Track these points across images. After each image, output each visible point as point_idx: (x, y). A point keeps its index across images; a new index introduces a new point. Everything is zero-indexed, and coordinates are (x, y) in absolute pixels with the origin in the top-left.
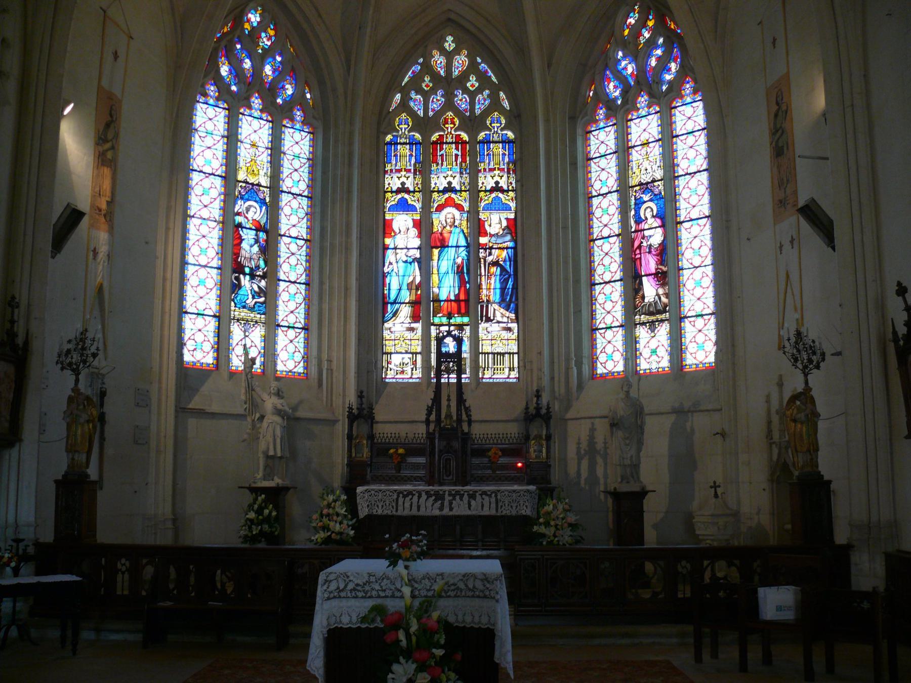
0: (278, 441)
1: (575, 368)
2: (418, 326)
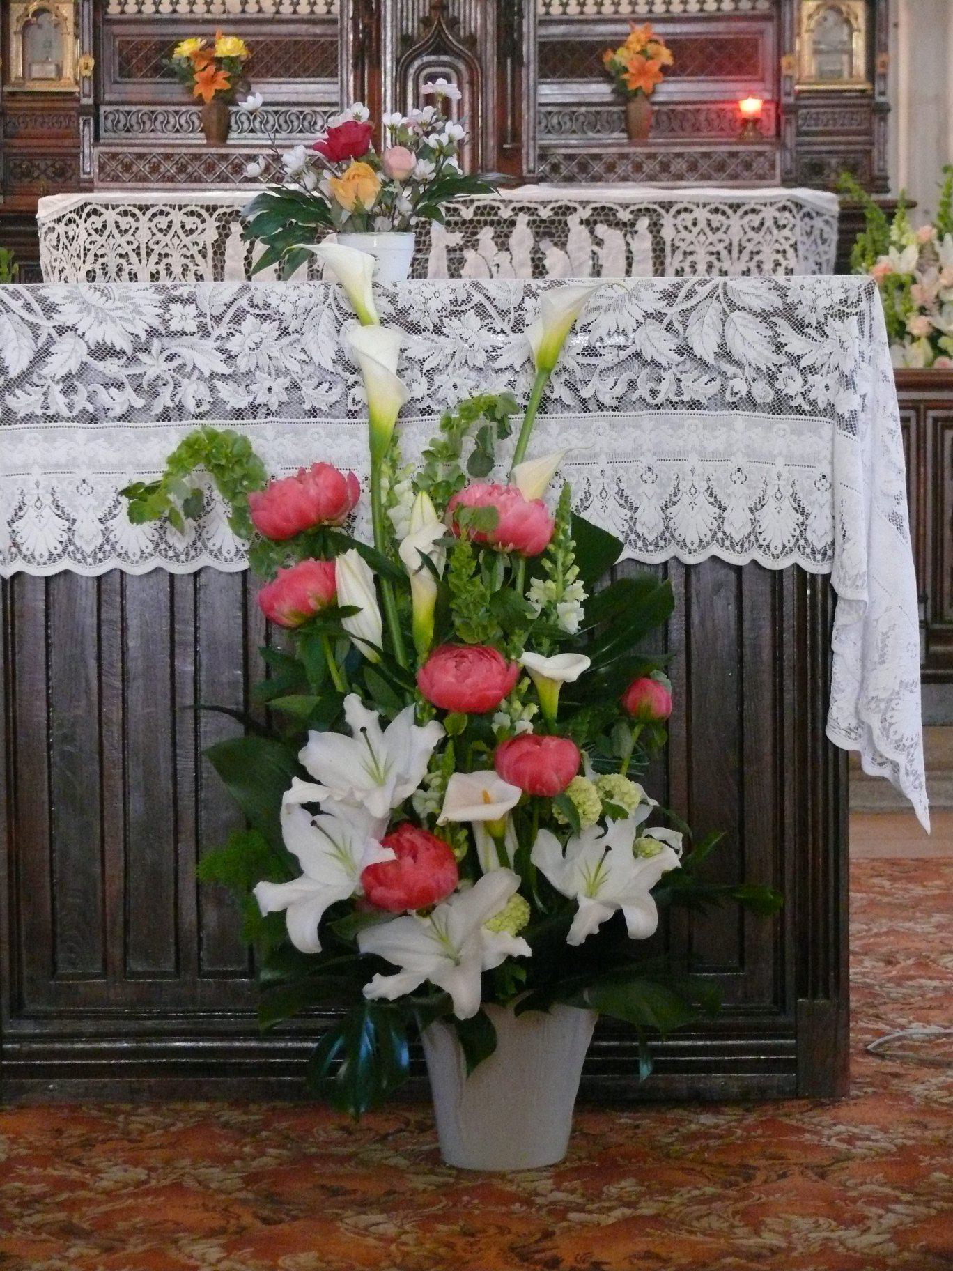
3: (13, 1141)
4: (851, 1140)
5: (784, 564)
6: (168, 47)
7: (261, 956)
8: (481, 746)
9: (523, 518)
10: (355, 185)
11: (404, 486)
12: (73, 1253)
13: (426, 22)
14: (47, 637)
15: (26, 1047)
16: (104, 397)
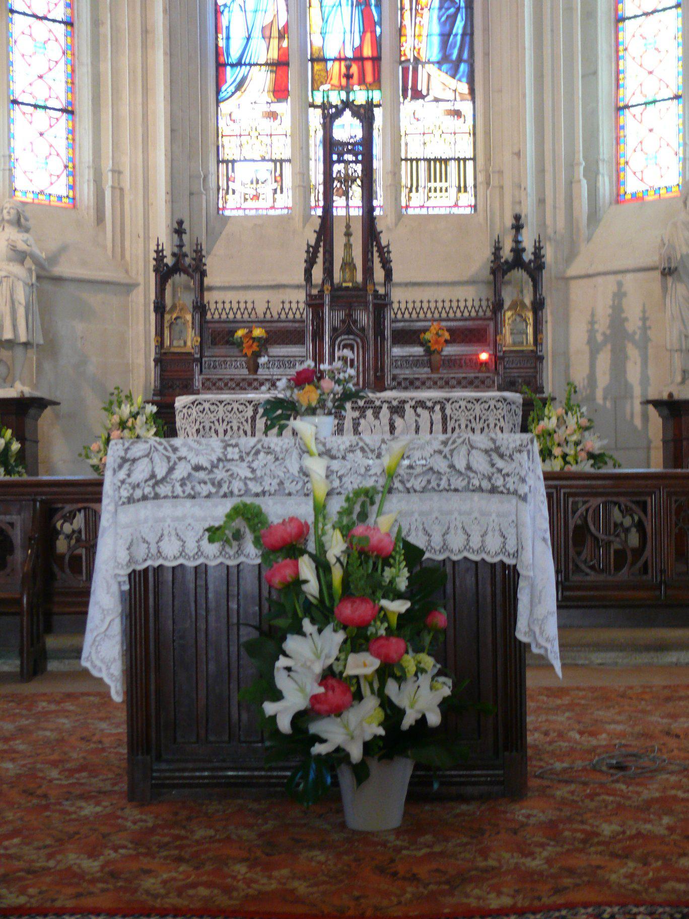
0: (21, 312)
1: (584, 182)
2: (284, 109)
3: (156, 817)
4: (528, 817)
5: (496, 560)
6: (232, 332)
7: (266, 735)
8: (363, 641)
9: (380, 541)
10: (308, 396)
11: (329, 527)
12: (181, 869)
13: (343, 321)
14: (173, 593)
15: (163, 775)
16: (198, 488)
